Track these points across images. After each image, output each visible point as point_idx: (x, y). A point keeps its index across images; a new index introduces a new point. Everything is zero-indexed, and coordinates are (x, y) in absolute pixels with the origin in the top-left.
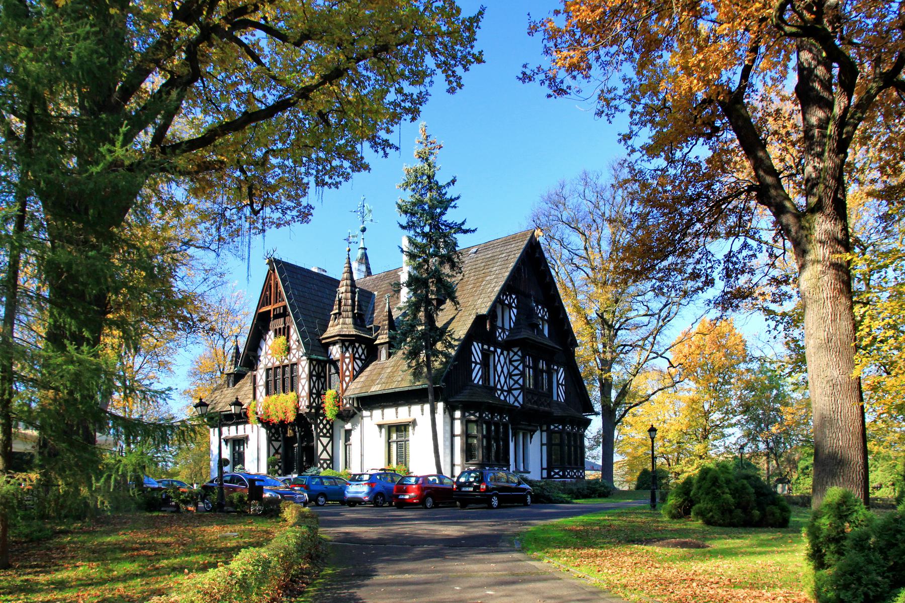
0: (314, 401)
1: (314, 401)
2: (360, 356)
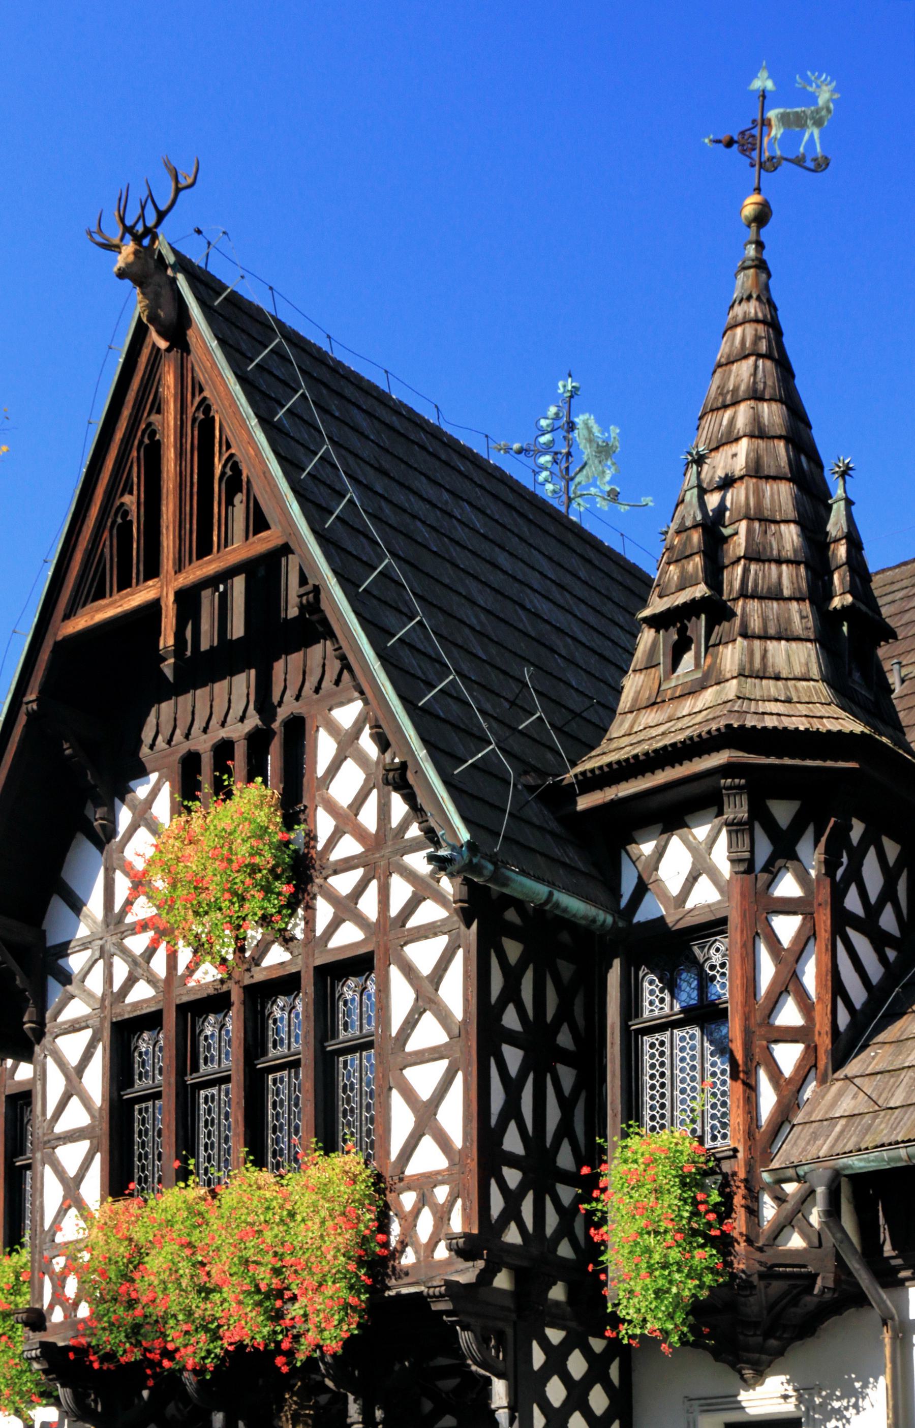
0: (512, 1212)
1: (512, 1212)
2: (873, 911)
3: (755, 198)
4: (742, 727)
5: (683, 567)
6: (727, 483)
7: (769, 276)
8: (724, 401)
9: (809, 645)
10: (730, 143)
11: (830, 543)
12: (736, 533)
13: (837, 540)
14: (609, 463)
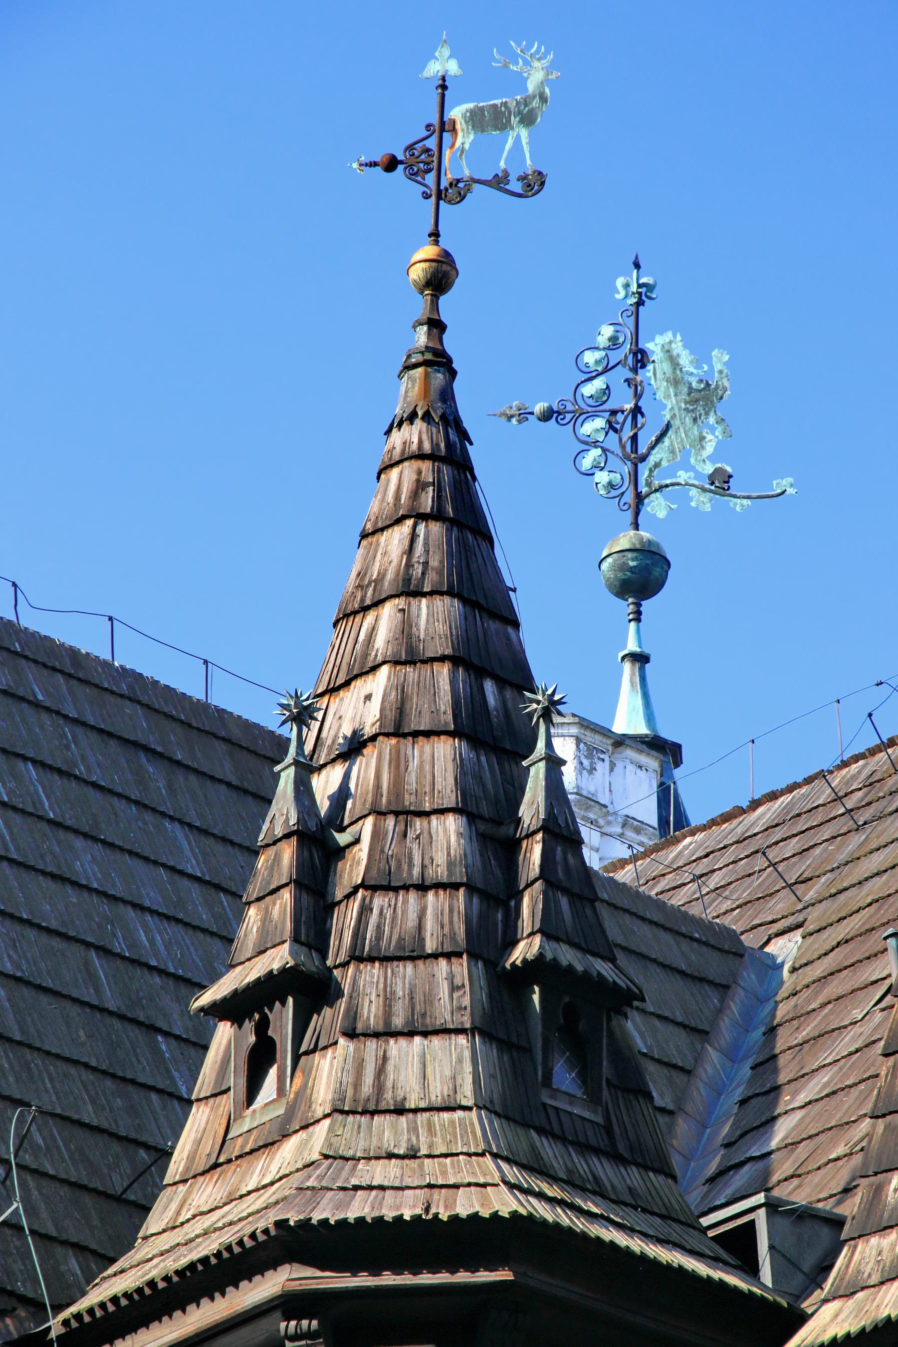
3: (429, 251)
4: (305, 1224)
5: (267, 909)
6: (355, 747)
7: (453, 373)
8: (363, 600)
9: (462, 1040)
10: (391, 164)
11: (520, 840)
12: (357, 841)
13: (530, 835)
14: (712, 420)
